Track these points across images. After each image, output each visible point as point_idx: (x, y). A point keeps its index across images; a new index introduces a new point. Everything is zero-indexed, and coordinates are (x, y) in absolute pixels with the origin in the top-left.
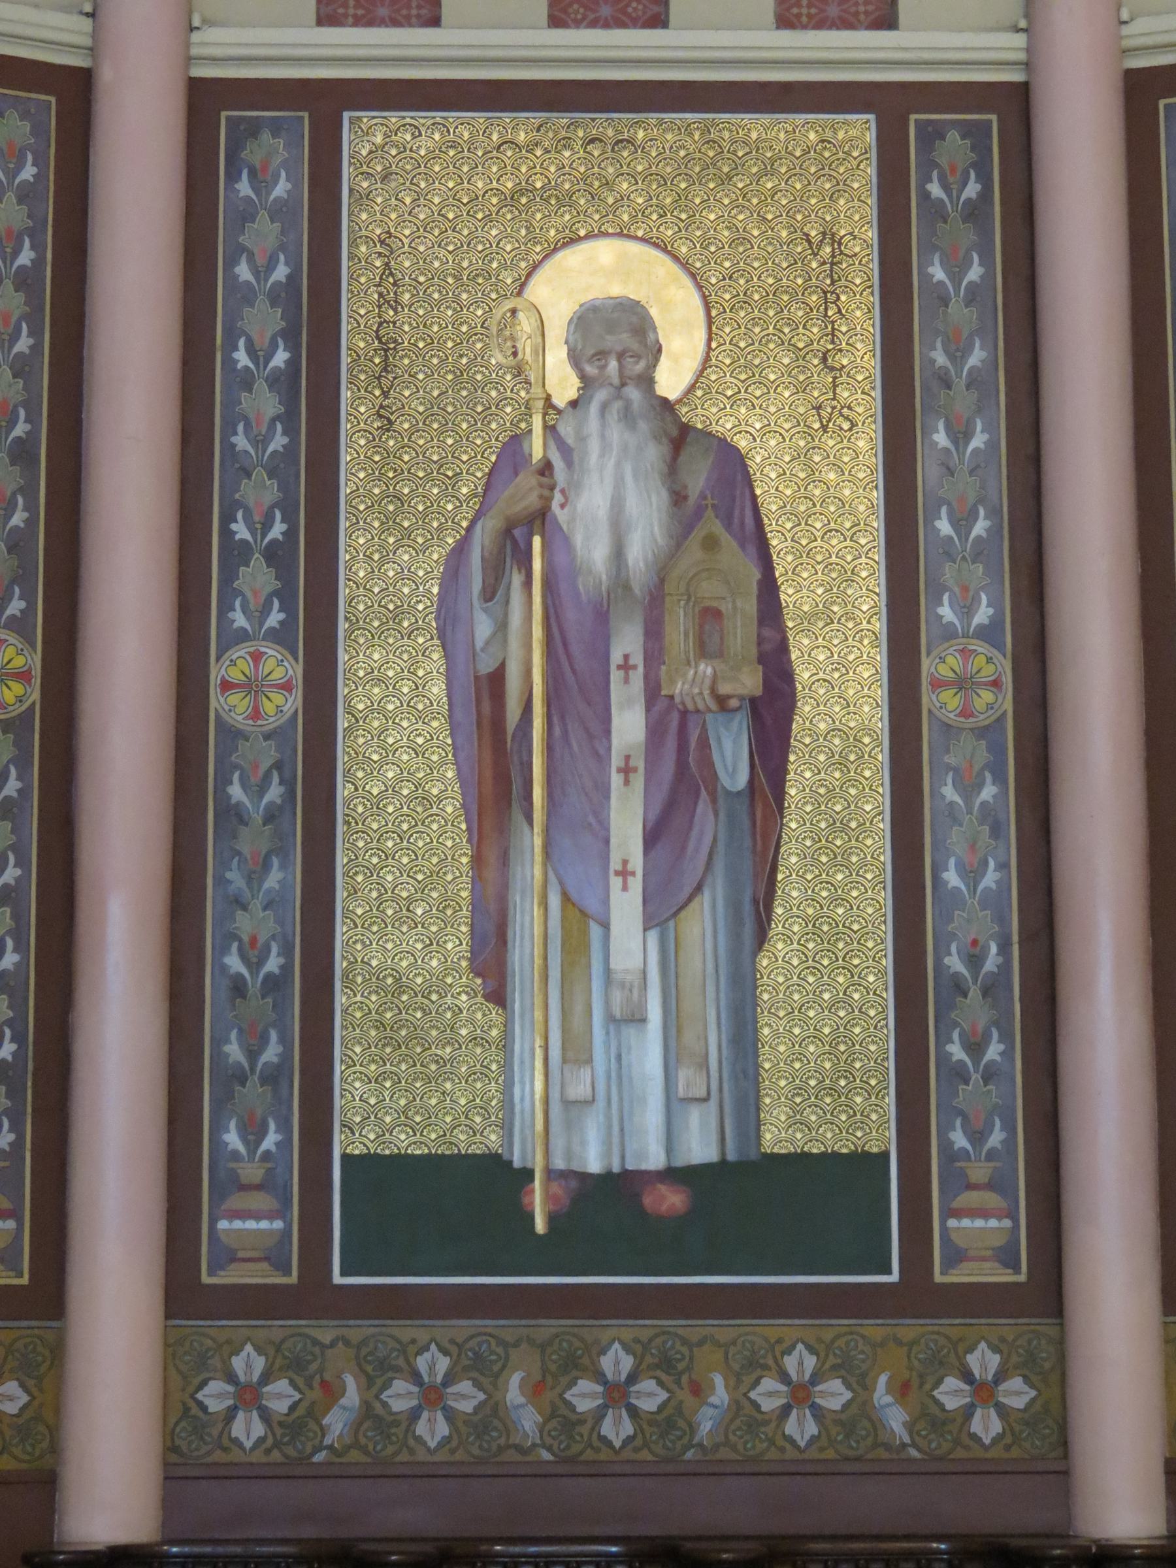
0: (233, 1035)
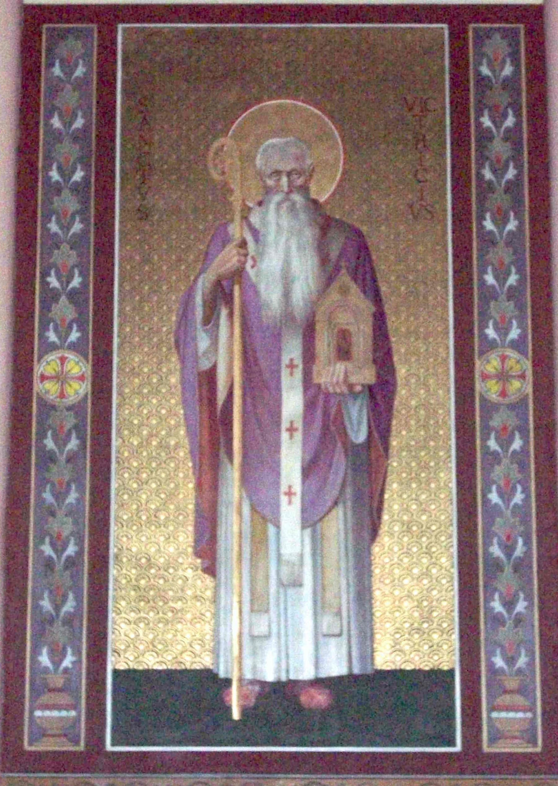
0: (46, 595)
